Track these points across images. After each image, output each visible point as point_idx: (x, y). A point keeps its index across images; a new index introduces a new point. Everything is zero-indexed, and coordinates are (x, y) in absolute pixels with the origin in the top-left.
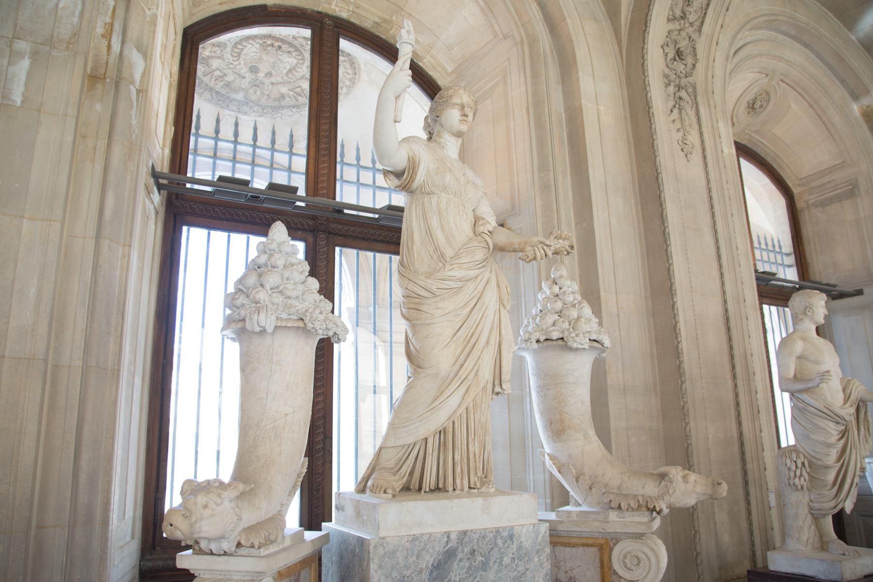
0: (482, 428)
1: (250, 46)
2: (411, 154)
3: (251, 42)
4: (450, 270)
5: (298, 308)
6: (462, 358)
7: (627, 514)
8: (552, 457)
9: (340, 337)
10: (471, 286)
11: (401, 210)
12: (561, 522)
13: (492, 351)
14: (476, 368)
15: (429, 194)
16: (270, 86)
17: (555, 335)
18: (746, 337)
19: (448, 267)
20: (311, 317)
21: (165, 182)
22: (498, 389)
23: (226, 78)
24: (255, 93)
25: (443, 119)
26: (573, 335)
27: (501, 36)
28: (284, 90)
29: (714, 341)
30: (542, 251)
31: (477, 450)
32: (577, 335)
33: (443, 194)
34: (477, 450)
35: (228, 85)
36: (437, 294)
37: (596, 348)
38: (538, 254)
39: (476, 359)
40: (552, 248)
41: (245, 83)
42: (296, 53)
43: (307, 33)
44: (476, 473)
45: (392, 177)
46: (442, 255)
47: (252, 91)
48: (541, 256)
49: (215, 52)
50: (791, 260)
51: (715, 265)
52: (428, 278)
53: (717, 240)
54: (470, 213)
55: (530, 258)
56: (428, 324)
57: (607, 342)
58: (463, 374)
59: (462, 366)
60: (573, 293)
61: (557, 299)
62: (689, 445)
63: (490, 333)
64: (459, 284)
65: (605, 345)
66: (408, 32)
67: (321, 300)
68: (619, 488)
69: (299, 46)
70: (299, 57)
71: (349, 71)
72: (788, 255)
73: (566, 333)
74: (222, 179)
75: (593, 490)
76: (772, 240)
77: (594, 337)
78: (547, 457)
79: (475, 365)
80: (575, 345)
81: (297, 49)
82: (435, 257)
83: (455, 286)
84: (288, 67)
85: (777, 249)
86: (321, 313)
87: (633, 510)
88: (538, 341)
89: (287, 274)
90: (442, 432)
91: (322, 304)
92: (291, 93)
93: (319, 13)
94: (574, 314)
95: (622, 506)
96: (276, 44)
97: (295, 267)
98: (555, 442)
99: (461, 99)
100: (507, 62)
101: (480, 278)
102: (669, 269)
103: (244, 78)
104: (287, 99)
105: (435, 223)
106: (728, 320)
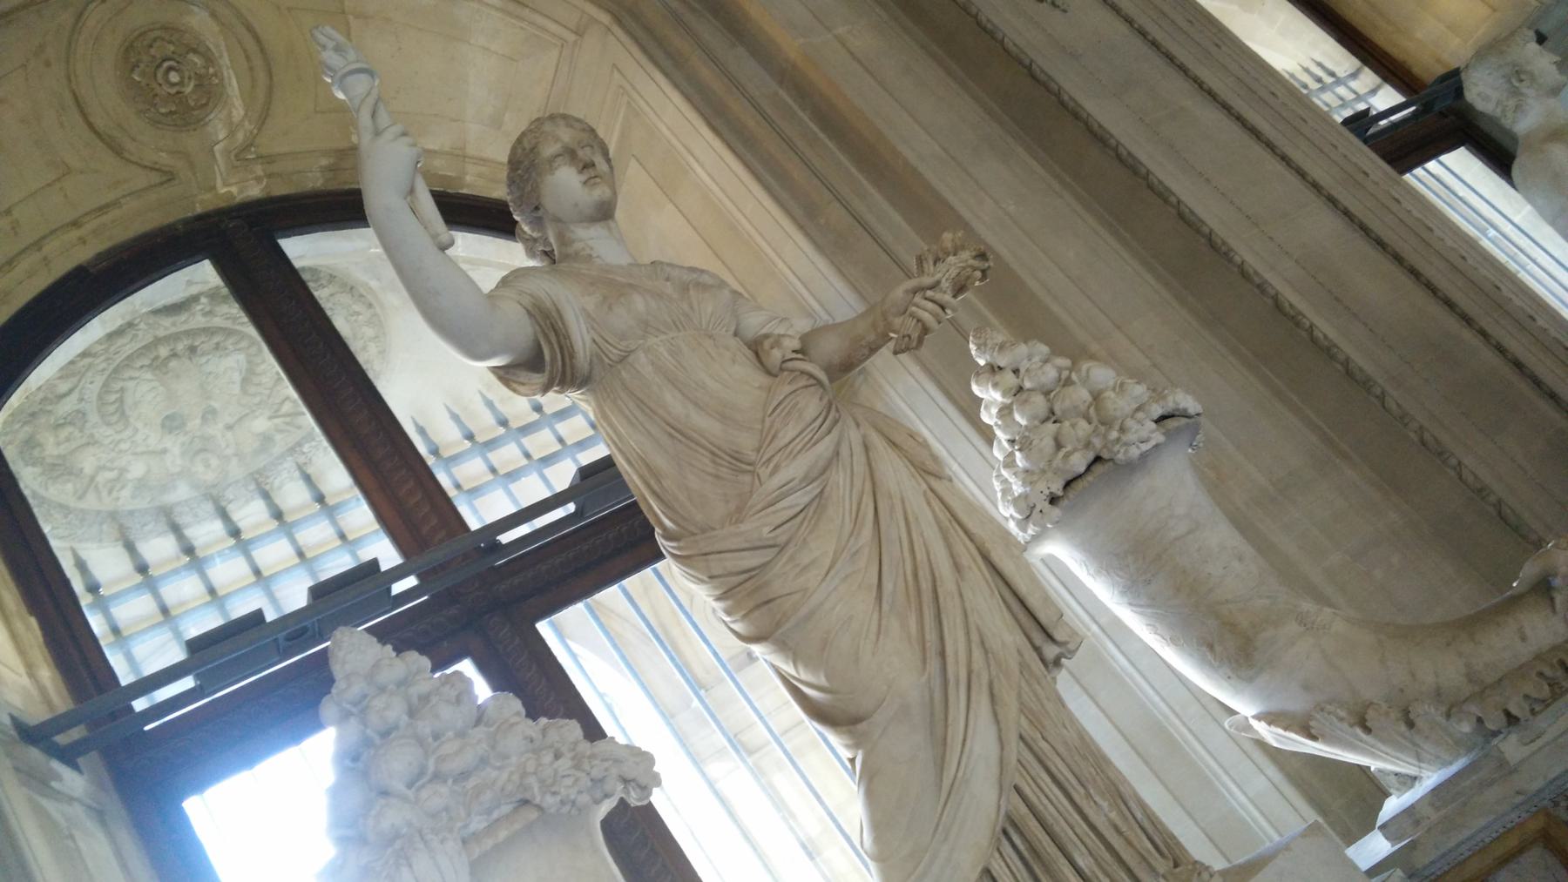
0: (1085, 758)
1: (131, 384)
2: (526, 301)
3: (128, 373)
4: (773, 473)
5: (499, 784)
6: (931, 636)
7: (1541, 722)
8: (1271, 718)
9: (643, 781)
10: (839, 478)
11: (606, 464)
12: (1412, 846)
13: (977, 574)
14: (975, 637)
15: (623, 359)
16: (229, 434)
17: (1079, 462)
18: (1425, 234)
19: (764, 472)
20: (542, 782)
21: (77, 733)
22: (1051, 651)
23: (129, 476)
24: (208, 466)
25: (549, 203)
26: (1114, 434)
27: (572, 37)
28: (261, 424)
29: (1374, 284)
30: (930, 305)
31: (1113, 815)
32: (1122, 430)
33: (652, 341)
34: (1113, 815)
35: (142, 485)
36: (782, 540)
37: (1178, 430)
38: (926, 316)
39: (959, 620)
40: (945, 284)
41: (174, 461)
42: (231, 341)
43: (204, 275)
44: (1153, 870)
45: (524, 376)
46: (737, 457)
47: (199, 468)
48: (935, 315)
49: (68, 440)
50: (1369, 78)
51: (1258, 150)
52: (739, 521)
53: (1226, 108)
54: (734, 343)
55: (915, 335)
56: (808, 617)
57: (1190, 404)
58: (957, 670)
59: (942, 654)
60: (1046, 361)
61: (1024, 396)
62: (1499, 504)
63: (946, 539)
64: (814, 489)
65: (1192, 411)
66: (338, 49)
67: (544, 731)
68: (1471, 677)
69: (228, 324)
70: (244, 344)
71: (356, 308)
72: (1354, 75)
73: (1097, 442)
74: (196, 646)
75: (1419, 723)
76: (1307, 70)
77: (1157, 411)
78: (1255, 724)
79: (968, 633)
80: (1134, 452)
81: (229, 333)
82: (724, 472)
83: (806, 499)
84: (237, 377)
85: (1329, 80)
86: (557, 756)
87: (1546, 703)
88: (1053, 500)
89: (425, 727)
90: (1009, 828)
91: (553, 736)
92: (277, 421)
93: (200, 218)
94: (1081, 395)
95: (1514, 711)
96: (180, 347)
97: (434, 700)
98: (1250, 680)
99: (557, 139)
100: (616, 75)
101: (844, 451)
102: (1181, 216)
103: (164, 451)
104: (278, 437)
105: (674, 403)
106: (1364, 229)
